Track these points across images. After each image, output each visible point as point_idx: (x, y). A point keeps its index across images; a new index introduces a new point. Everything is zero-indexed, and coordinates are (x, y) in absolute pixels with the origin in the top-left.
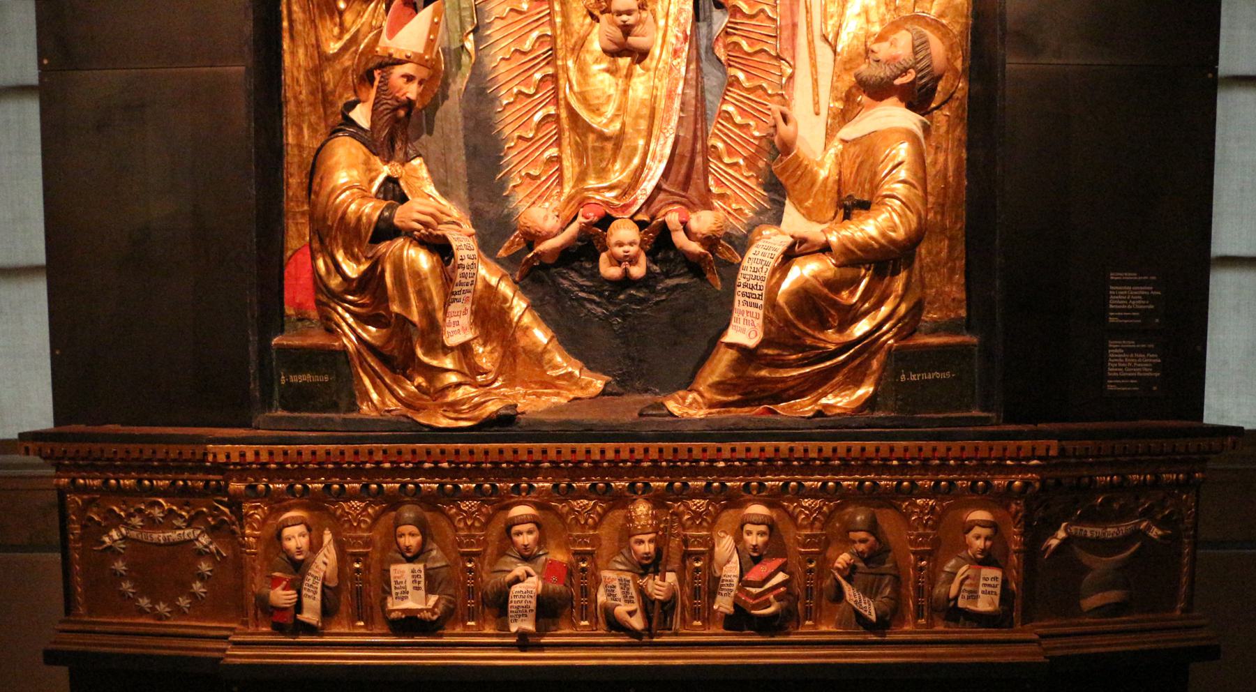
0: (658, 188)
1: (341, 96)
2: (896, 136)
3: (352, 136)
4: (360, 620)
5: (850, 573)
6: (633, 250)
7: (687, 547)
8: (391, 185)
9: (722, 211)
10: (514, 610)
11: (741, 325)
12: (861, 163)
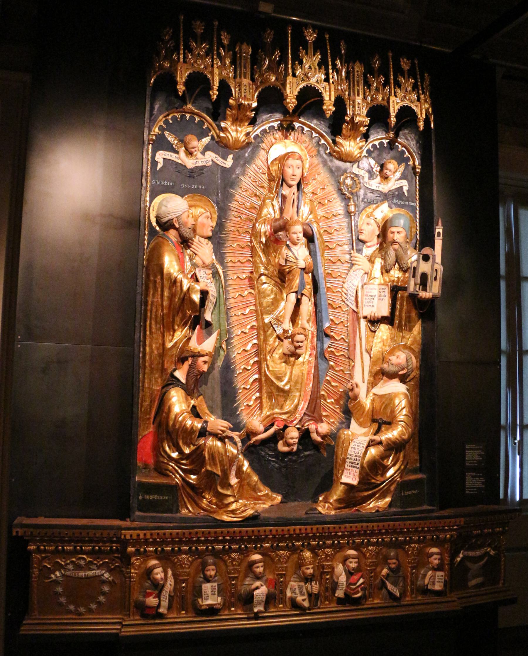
5: (387, 576)
11: (348, 475)
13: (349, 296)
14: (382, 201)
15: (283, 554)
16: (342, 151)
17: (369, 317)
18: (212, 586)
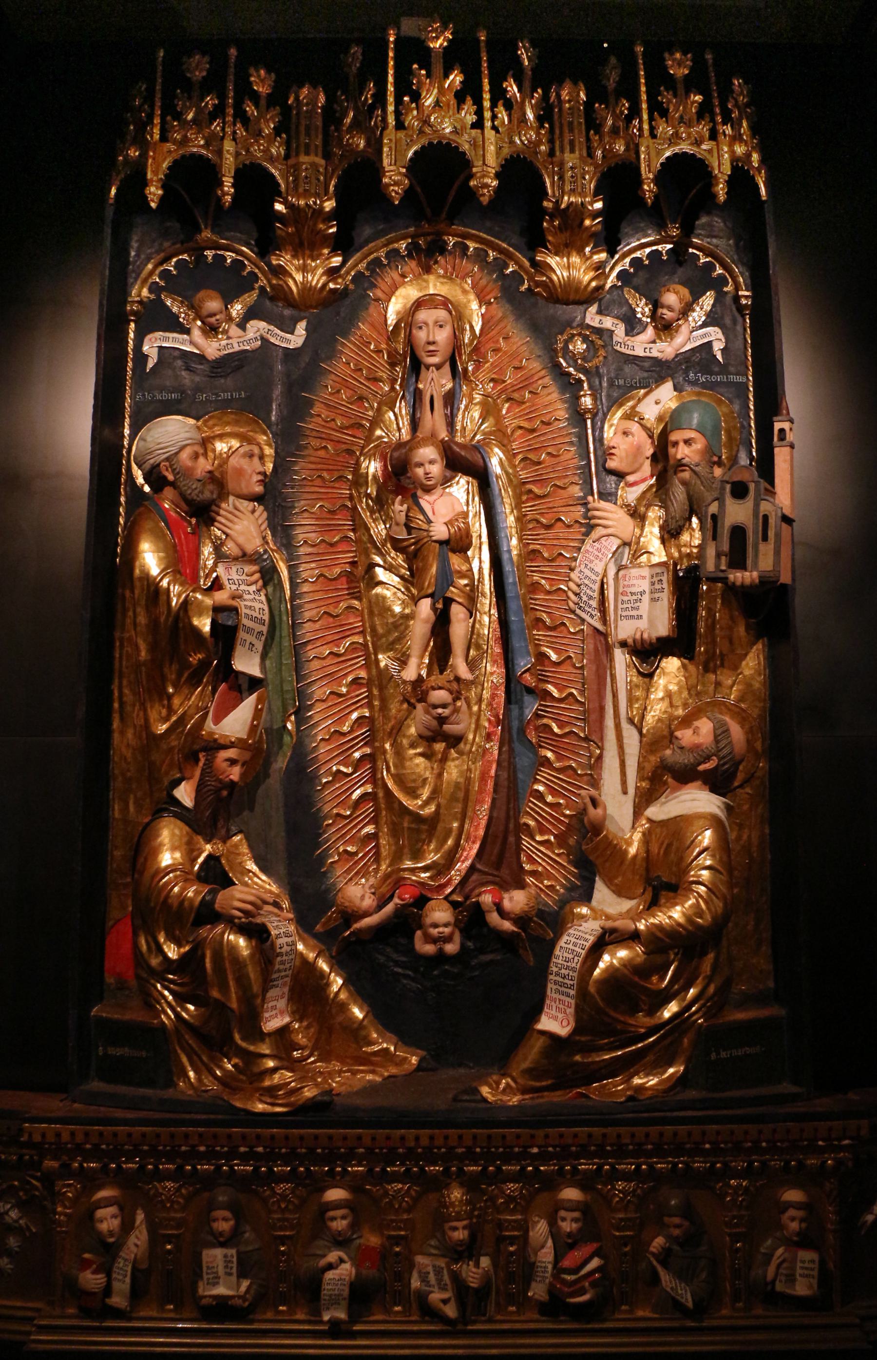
0: (472, 869)
1: (167, 773)
2: (701, 822)
3: (176, 816)
4: (170, 1303)
5: (665, 1257)
6: (447, 930)
7: (501, 1231)
8: (212, 863)
9: (534, 888)
10: (327, 1298)
11: (554, 1012)
12: (669, 845)
13: (585, 598)
14: (660, 381)
15: (400, 1190)
16: (551, 280)
17: (630, 641)
18: (225, 1256)
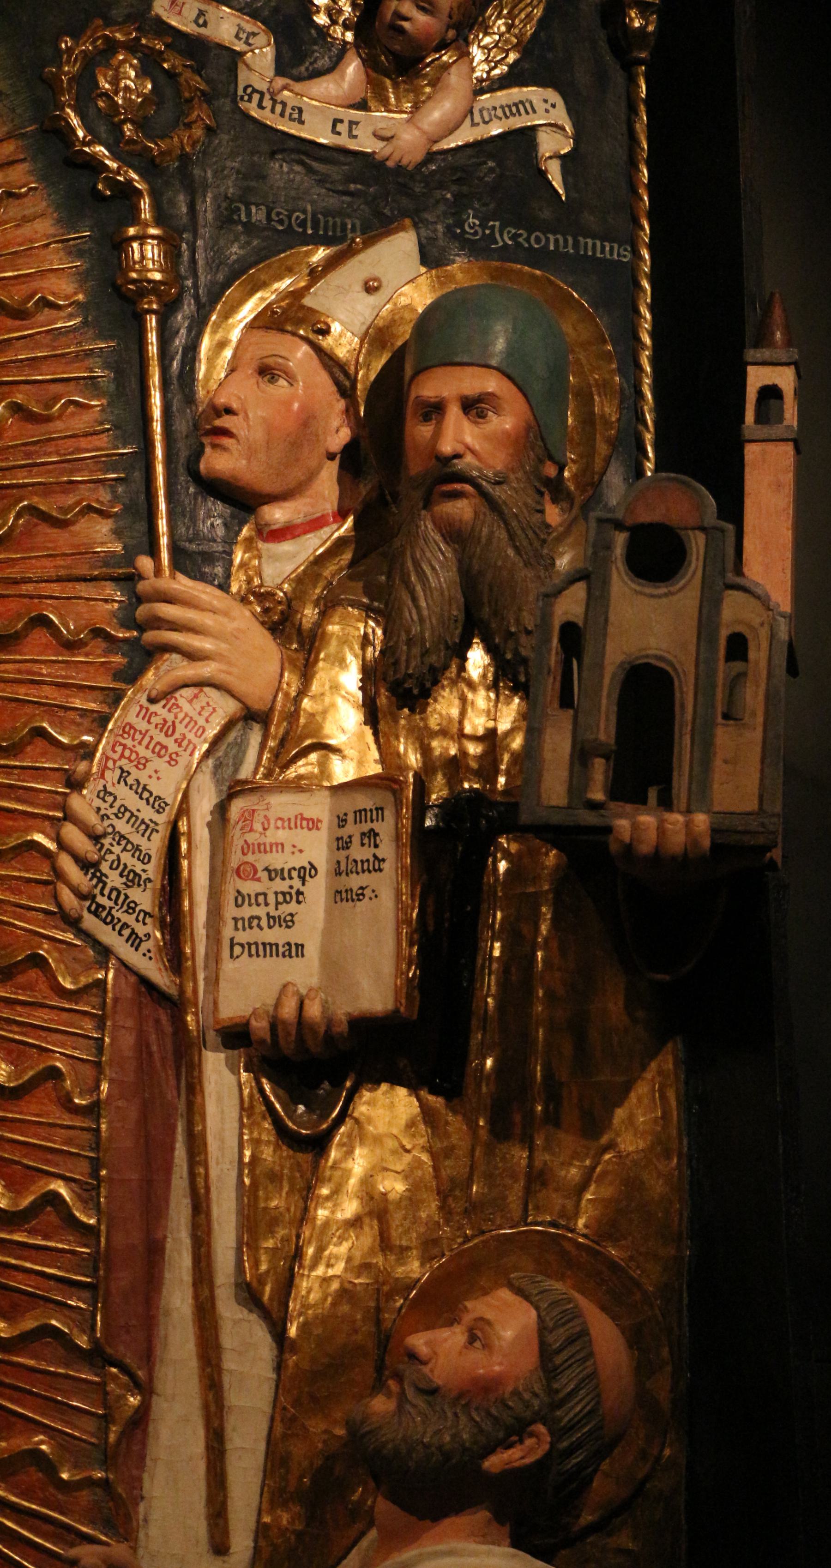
13: (114, 879)
17: (260, 1026)
